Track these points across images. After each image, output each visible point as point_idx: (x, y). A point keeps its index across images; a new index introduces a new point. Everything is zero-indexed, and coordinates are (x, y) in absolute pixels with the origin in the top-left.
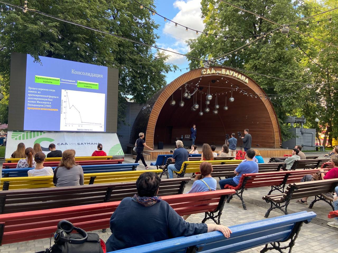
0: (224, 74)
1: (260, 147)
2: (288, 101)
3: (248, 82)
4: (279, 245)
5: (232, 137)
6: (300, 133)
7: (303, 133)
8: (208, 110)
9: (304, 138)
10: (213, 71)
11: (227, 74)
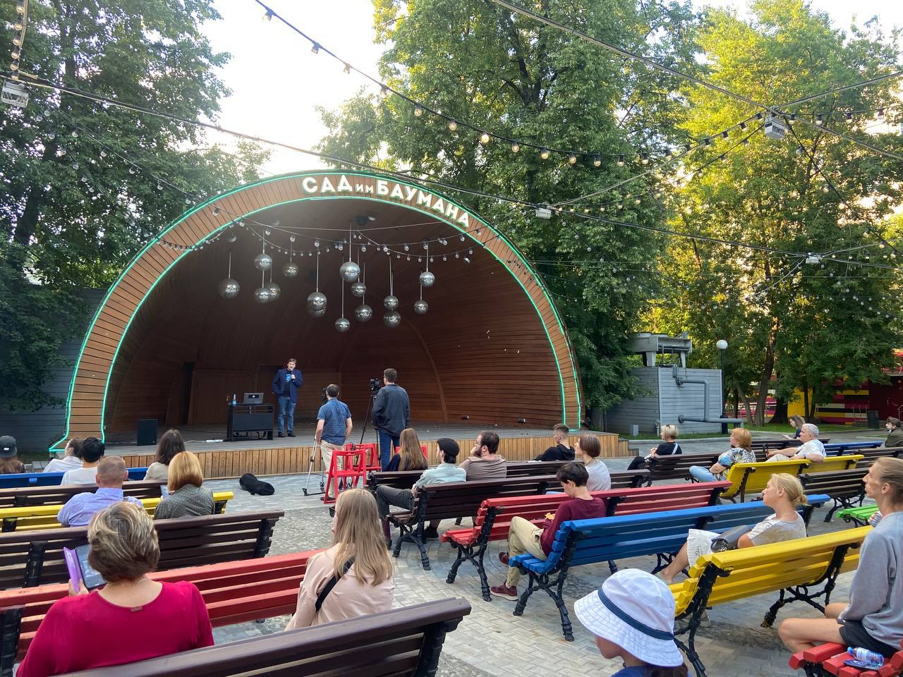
0: (385, 197)
1: (529, 428)
2: (598, 283)
3: (467, 224)
5: (329, 398)
7: (682, 383)
8: (365, 312)
9: (686, 396)
10: (344, 185)
11: (393, 195)
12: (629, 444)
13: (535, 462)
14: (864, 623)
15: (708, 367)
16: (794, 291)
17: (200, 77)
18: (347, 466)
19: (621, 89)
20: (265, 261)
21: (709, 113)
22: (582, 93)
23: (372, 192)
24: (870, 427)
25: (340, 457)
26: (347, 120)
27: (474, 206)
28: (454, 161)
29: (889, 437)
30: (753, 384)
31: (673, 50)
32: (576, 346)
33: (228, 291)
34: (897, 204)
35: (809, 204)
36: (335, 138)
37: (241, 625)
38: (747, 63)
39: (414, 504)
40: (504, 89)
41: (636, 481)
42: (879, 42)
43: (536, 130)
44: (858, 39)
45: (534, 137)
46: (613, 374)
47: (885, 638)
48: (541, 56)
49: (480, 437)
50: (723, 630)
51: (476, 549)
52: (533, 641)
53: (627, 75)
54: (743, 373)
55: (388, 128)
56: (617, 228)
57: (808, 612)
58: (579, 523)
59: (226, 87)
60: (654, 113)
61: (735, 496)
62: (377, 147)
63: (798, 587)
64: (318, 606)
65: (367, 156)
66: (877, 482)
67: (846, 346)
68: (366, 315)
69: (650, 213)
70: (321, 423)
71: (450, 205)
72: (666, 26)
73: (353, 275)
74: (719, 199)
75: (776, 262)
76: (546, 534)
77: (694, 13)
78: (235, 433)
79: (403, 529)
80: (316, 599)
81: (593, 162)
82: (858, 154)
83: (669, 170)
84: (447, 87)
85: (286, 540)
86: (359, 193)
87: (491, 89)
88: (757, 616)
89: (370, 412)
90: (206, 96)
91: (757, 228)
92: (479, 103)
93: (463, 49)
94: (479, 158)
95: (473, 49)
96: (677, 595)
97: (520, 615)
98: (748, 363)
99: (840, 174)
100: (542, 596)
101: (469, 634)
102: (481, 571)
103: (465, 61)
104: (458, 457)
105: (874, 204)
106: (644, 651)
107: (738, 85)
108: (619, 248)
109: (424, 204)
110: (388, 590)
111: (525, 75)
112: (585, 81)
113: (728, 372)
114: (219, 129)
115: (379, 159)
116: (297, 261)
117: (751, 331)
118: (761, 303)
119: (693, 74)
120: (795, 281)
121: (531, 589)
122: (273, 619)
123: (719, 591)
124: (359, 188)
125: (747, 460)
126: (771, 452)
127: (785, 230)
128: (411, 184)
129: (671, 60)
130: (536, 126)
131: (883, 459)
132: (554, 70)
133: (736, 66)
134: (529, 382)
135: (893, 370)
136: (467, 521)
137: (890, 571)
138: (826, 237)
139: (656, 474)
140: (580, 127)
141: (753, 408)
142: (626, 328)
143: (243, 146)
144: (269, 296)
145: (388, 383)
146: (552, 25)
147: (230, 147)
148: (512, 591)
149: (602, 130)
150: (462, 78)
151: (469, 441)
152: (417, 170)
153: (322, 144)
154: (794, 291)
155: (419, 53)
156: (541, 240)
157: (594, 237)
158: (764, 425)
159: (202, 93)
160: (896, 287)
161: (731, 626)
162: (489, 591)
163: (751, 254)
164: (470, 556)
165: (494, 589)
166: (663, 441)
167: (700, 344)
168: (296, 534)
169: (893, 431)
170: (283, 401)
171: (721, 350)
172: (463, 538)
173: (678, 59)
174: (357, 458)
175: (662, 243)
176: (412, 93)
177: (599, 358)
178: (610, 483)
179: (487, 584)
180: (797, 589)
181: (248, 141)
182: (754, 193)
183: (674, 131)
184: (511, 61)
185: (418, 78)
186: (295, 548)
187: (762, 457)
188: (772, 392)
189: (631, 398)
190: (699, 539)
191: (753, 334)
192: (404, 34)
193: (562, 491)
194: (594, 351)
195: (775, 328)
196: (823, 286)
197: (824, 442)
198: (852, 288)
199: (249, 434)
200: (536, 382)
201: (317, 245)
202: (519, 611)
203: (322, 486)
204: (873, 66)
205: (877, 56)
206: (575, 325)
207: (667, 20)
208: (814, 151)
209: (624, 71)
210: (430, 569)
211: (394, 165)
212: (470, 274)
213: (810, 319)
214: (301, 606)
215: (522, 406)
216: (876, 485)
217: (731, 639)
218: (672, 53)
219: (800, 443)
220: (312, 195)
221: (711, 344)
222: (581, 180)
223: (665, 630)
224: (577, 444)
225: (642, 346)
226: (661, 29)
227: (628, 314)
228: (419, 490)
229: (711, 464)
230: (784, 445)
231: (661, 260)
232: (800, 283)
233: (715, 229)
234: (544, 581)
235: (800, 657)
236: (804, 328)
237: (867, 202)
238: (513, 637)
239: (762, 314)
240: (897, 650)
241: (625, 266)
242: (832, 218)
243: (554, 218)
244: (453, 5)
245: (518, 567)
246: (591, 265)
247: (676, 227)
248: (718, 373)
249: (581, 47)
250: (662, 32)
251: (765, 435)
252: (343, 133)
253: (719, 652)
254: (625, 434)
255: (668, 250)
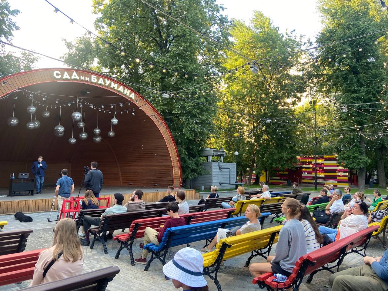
0: (95, 83)
1: (159, 188)
2: (189, 127)
4: (261, 251)
5: (63, 175)
6: (218, 168)
7: (221, 169)
9: (223, 174)
10: (75, 76)
11: (99, 82)
12: (200, 194)
13: (159, 203)
14: (280, 263)
15: (231, 162)
16: (262, 133)
17: (3, 19)
18: (71, 208)
19: (200, 47)
20: (33, 109)
21: (234, 61)
22: (184, 47)
23: (89, 80)
24: (288, 186)
25: (68, 203)
26: (78, 46)
27: (137, 91)
28: (129, 70)
29: (294, 190)
30: (248, 169)
31: (221, 34)
32: (179, 153)
33: (12, 123)
34: (299, 102)
35: (269, 100)
36: (72, 54)
37: (9, 285)
38: (248, 43)
39: (101, 224)
40: (152, 41)
41: (200, 209)
42: (295, 40)
43: (165, 60)
44: (288, 38)
45: (164, 63)
46: (194, 165)
47: (287, 269)
48: (168, 29)
49: (134, 192)
50: (230, 270)
51: (129, 242)
52: (151, 282)
53: (203, 42)
54: (244, 165)
55: (98, 52)
56: (197, 104)
57: (262, 260)
58: (173, 229)
59: (17, 26)
60: (213, 59)
61: (238, 214)
62: (93, 60)
63: (258, 250)
64: (44, 275)
65: (88, 64)
66: (286, 207)
67: (280, 155)
68: (84, 137)
69: (210, 100)
70: (58, 187)
71: (126, 89)
72: (218, 24)
73: (78, 118)
74: (237, 96)
75: (257, 121)
76: (159, 234)
77: (229, 20)
78: (13, 192)
79: (96, 235)
80: (43, 271)
81: (189, 75)
82: (286, 82)
83: (218, 82)
84: (126, 37)
85: (37, 243)
86: (82, 80)
87: (146, 40)
88: (243, 263)
89: (83, 182)
90: (6, 29)
91: (250, 108)
92: (141, 46)
93: (134, 22)
94: (140, 70)
95: (138, 22)
96: (211, 257)
97: (147, 270)
98: (246, 161)
99: (280, 89)
100: (157, 261)
101: (123, 281)
102: (131, 253)
103: (135, 27)
104: (123, 202)
105: (291, 101)
106: (189, 282)
107: (244, 51)
108: (198, 113)
109: (114, 88)
110: (80, 265)
111: (161, 36)
112: (186, 42)
113: (238, 164)
114: (11, 45)
115: (93, 66)
116: (49, 110)
117: (247, 148)
118: (251, 137)
119: (228, 45)
120: (263, 129)
121: (152, 259)
122: (26, 281)
123: (227, 253)
124: (83, 78)
125: (243, 199)
126: (252, 196)
127: (260, 109)
128: (108, 78)
129: (219, 38)
130: (165, 59)
131: (288, 198)
132: (173, 36)
133: (244, 44)
134: (160, 168)
135: (296, 164)
136: (127, 230)
137: (289, 242)
138: (274, 113)
139: (208, 206)
140: (183, 61)
141: (247, 179)
142: (200, 146)
143: (24, 54)
144: (35, 126)
145: (93, 168)
146: (172, 18)
147: (17, 54)
148: (144, 260)
149: (192, 64)
150: (133, 34)
151: (129, 195)
152: (111, 72)
153: (65, 56)
154: (262, 133)
155: (113, 20)
156: (166, 107)
157: (188, 107)
158: (251, 185)
159: (4, 27)
160: (298, 133)
161: (233, 268)
162: (134, 261)
163: (248, 118)
164: (126, 246)
165: (136, 260)
166: (212, 192)
167: (229, 153)
168: (42, 241)
169: (295, 187)
170: (37, 177)
171: (236, 155)
172: (123, 238)
173: (222, 38)
174: (76, 203)
175: (215, 112)
176: (110, 38)
177: (189, 158)
178: (189, 211)
179: (133, 258)
180: (258, 251)
181: (27, 52)
182: (249, 94)
183: (221, 67)
184: (155, 30)
185: (112, 31)
186: (41, 247)
187: (248, 198)
188: (254, 172)
189: (201, 175)
190: (222, 232)
191: (248, 149)
192: (107, 11)
193: (168, 215)
194: (187, 155)
195: (256, 147)
196: (273, 132)
197: (271, 192)
198: (282, 133)
199: (21, 192)
200: (162, 168)
201: (57, 102)
202: (146, 269)
203: (58, 217)
204: (293, 49)
205: (294, 45)
206: (179, 144)
207: (219, 22)
208: (271, 79)
209: (202, 40)
210: (107, 253)
211: (101, 69)
212: (134, 120)
213: (268, 144)
214: (35, 275)
215: (156, 178)
216: (285, 208)
217: (233, 273)
218: (220, 36)
219: (261, 192)
220: (58, 79)
221: (233, 153)
222: (183, 83)
223: (198, 271)
224: (176, 195)
225: (206, 153)
226: (216, 25)
227: (201, 140)
228: (104, 217)
229: (230, 201)
230: (257, 193)
231: (215, 119)
232: (265, 130)
233: (235, 108)
234: (158, 255)
235: (256, 279)
236: (266, 147)
237: (289, 101)
238: (143, 281)
239: (251, 142)
240: (291, 274)
241: (200, 120)
242: (276, 105)
243: (171, 99)
244: (130, 2)
245: (147, 249)
246: (187, 119)
247: (221, 106)
248: (235, 165)
249: (184, 28)
250: (216, 26)
251: (251, 189)
252: (75, 52)
253: (228, 279)
254: (198, 189)
255: (218, 115)
